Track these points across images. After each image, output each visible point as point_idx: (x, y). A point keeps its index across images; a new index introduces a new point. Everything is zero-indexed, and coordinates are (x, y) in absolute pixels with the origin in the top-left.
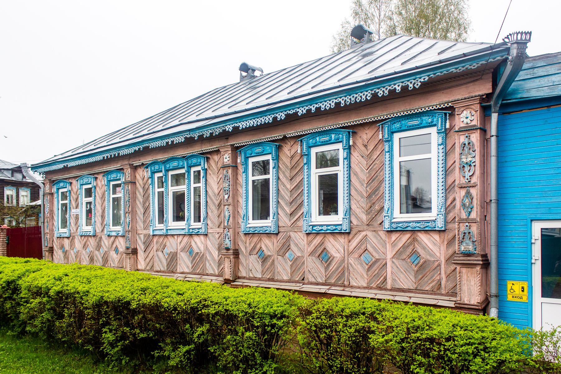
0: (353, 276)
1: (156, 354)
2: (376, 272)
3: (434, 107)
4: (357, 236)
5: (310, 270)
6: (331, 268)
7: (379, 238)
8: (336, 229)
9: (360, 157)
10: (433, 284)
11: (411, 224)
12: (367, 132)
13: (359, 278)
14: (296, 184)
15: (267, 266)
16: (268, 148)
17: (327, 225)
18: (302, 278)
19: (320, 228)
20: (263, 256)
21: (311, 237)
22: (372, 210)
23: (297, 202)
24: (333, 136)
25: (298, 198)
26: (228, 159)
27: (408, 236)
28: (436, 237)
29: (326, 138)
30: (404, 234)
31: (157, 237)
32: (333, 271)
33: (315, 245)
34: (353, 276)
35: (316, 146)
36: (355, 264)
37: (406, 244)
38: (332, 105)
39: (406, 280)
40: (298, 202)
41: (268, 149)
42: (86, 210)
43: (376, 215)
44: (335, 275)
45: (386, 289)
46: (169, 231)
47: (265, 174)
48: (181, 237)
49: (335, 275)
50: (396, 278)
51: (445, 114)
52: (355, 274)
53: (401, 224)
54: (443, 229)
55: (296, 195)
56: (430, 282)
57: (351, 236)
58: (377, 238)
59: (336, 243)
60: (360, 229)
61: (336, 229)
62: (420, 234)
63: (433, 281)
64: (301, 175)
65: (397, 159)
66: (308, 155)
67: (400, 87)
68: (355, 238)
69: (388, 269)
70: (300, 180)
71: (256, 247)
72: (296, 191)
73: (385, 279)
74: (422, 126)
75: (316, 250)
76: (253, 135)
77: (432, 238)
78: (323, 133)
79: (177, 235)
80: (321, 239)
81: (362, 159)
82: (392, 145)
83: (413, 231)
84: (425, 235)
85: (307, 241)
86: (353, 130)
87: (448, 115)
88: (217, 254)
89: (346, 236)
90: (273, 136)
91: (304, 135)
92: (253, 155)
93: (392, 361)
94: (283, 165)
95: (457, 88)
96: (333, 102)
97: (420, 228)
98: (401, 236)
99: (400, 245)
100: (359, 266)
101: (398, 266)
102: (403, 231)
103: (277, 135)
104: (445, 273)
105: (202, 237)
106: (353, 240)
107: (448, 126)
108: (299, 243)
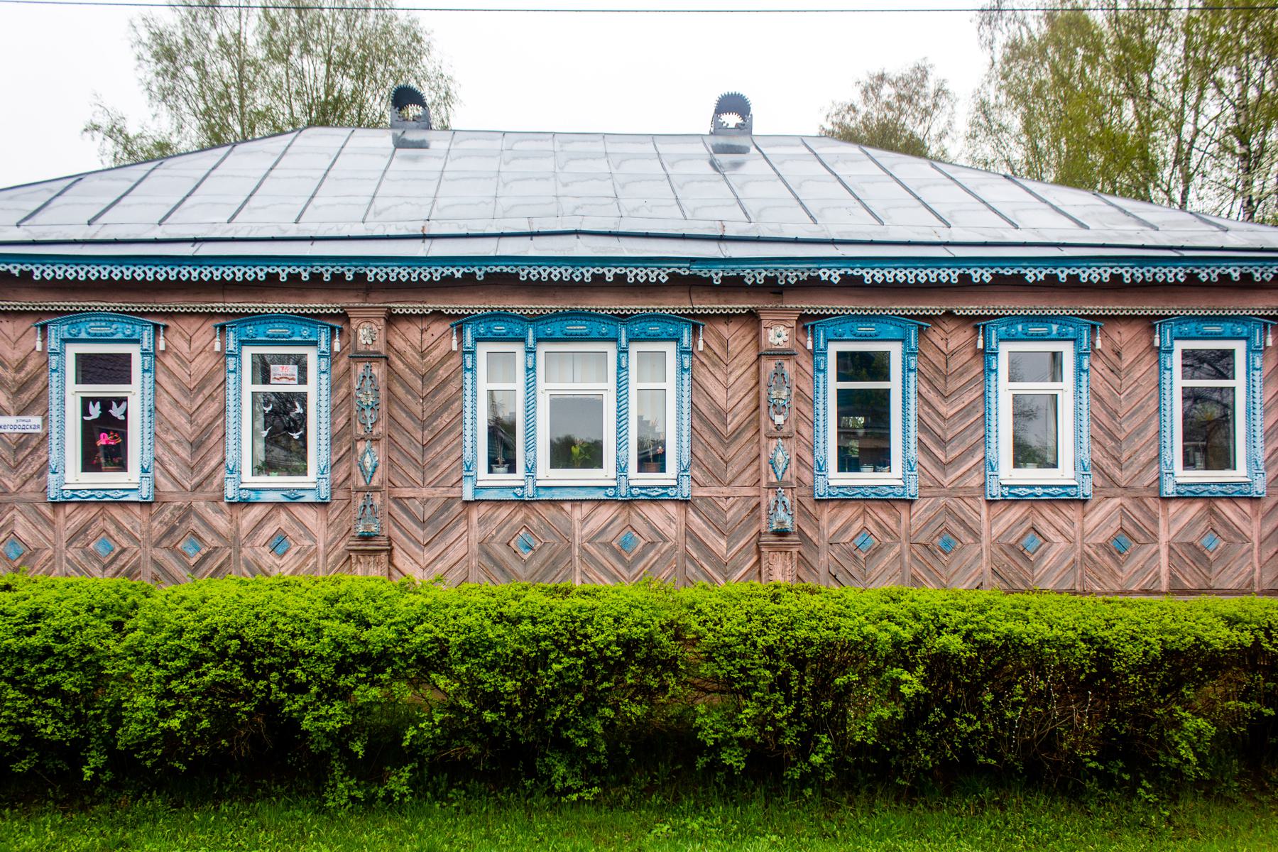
0: (1093, 575)
1: (154, 793)
2: (1139, 566)
3: (1257, 312)
4: (1101, 505)
5: (996, 569)
6: (1045, 563)
7: (1145, 509)
8: (91, 496)
9: (1108, 371)
10: (1241, 578)
11: (669, 491)
12: (1122, 330)
13: (1106, 578)
14: (963, 405)
15: (881, 566)
16: (892, 328)
17: (1043, 487)
18: (977, 584)
19: (1029, 491)
20: (869, 545)
21: (996, 509)
22: (1132, 463)
23: (964, 441)
24: (1055, 327)
25: (968, 432)
26: (786, 338)
27: (1198, 506)
28: (1246, 507)
29: (1042, 330)
30: (1191, 503)
31: (483, 509)
32: (1051, 568)
33: (1009, 520)
34: (1093, 575)
35: (75, 340)
36: (1097, 554)
37: (1195, 519)
38: (413, 275)
39: (1195, 575)
40: (967, 441)
41: (892, 330)
42: (84, 423)
43: (1140, 472)
44: (1055, 574)
45: (1158, 593)
46: (541, 492)
47: (1054, 380)
48: (586, 508)
49: (1055, 574)
50: (1178, 574)
51: (1094, 327)
52: (1097, 571)
53: (1193, 488)
54: (150, 500)
55: (962, 428)
56: (1236, 575)
57: (1088, 506)
58: (1141, 510)
59: (1056, 517)
60: (1108, 495)
61: (91, 496)
62: (1219, 504)
63: (1241, 574)
64: (974, 390)
65: (483, 386)
66: (238, 356)
67: (352, 272)
68: (1097, 509)
69: (1161, 560)
70: (972, 399)
71: (850, 526)
72: (962, 419)
73: (1157, 575)
74: (115, 337)
75: (1011, 532)
76: (858, 296)
77: (1238, 509)
78: (889, 321)
79: (571, 501)
80: (1023, 510)
81: (1112, 375)
82: (240, 362)
83: (1211, 499)
84: (1228, 504)
85: (988, 514)
86: (925, 322)
87: (1269, 327)
88: (725, 545)
89: (1079, 505)
90: (286, 305)
91: (992, 317)
92: (845, 337)
93: (1019, 703)
94: (928, 367)
95: (602, 291)
96: (327, 271)
97: (1068, 495)
98: (273, 512)
99: (1185, 520)
100: (1107, 558)
101: (1181, 554)
102: (1194, 498)
103: (934, 307)
104: (1260, 561)
105: (672, 509)
106: (1093, 513)
107: (980, 345)
108: (969, 518)
